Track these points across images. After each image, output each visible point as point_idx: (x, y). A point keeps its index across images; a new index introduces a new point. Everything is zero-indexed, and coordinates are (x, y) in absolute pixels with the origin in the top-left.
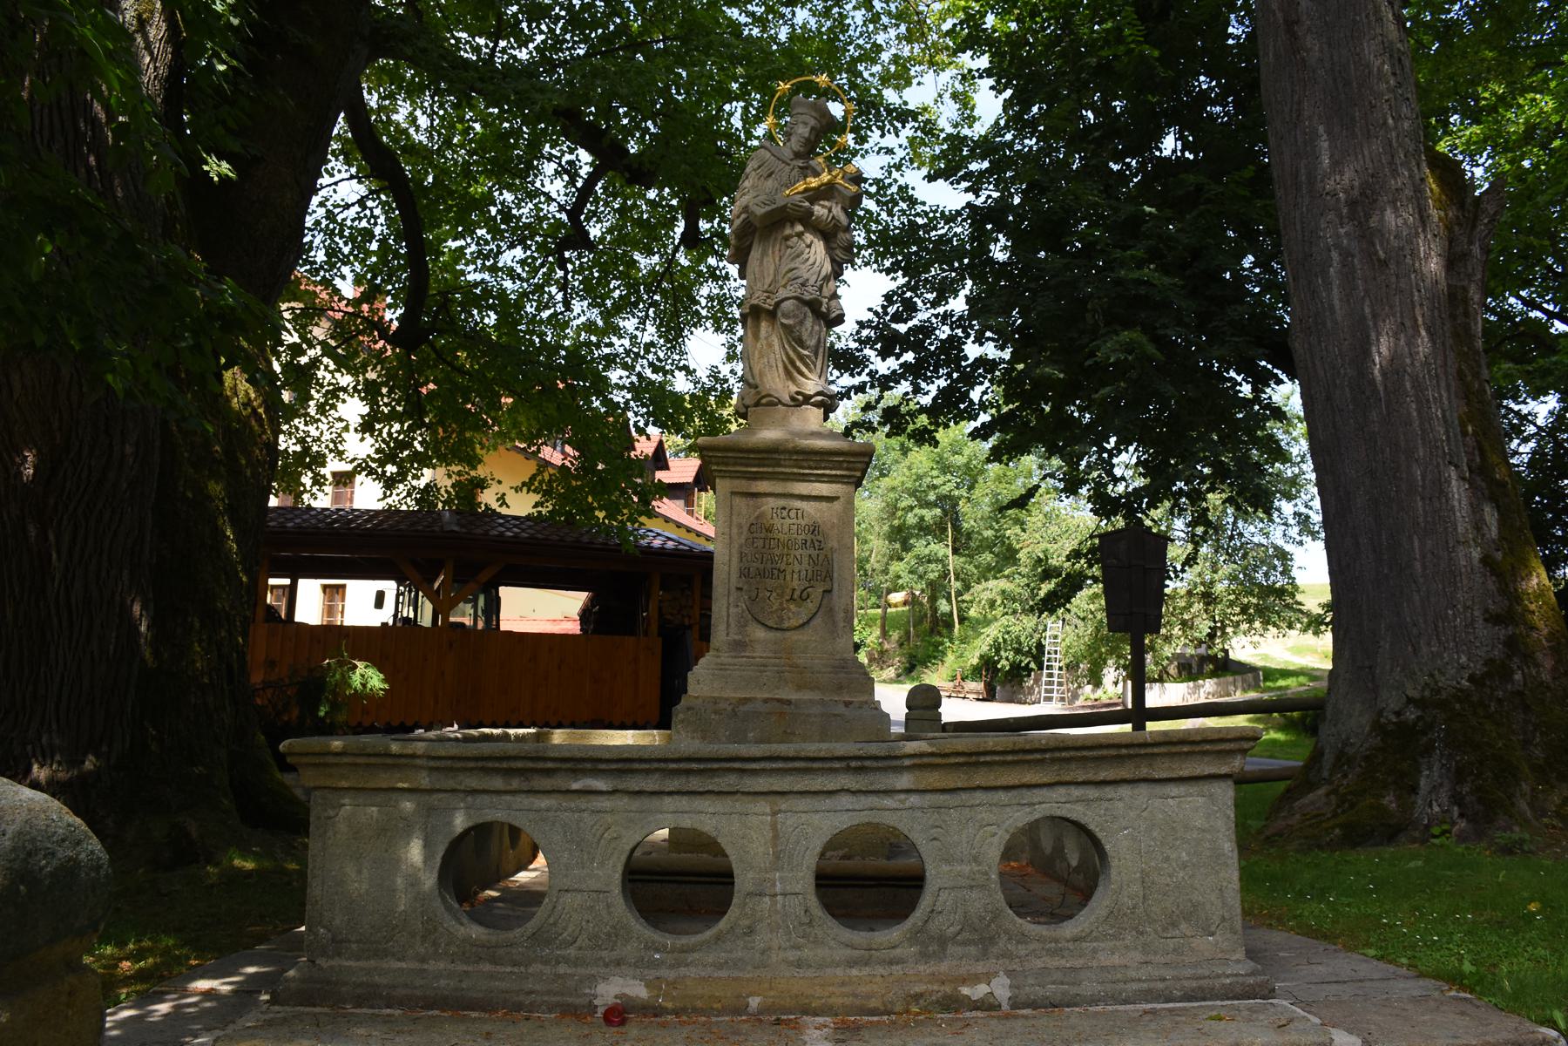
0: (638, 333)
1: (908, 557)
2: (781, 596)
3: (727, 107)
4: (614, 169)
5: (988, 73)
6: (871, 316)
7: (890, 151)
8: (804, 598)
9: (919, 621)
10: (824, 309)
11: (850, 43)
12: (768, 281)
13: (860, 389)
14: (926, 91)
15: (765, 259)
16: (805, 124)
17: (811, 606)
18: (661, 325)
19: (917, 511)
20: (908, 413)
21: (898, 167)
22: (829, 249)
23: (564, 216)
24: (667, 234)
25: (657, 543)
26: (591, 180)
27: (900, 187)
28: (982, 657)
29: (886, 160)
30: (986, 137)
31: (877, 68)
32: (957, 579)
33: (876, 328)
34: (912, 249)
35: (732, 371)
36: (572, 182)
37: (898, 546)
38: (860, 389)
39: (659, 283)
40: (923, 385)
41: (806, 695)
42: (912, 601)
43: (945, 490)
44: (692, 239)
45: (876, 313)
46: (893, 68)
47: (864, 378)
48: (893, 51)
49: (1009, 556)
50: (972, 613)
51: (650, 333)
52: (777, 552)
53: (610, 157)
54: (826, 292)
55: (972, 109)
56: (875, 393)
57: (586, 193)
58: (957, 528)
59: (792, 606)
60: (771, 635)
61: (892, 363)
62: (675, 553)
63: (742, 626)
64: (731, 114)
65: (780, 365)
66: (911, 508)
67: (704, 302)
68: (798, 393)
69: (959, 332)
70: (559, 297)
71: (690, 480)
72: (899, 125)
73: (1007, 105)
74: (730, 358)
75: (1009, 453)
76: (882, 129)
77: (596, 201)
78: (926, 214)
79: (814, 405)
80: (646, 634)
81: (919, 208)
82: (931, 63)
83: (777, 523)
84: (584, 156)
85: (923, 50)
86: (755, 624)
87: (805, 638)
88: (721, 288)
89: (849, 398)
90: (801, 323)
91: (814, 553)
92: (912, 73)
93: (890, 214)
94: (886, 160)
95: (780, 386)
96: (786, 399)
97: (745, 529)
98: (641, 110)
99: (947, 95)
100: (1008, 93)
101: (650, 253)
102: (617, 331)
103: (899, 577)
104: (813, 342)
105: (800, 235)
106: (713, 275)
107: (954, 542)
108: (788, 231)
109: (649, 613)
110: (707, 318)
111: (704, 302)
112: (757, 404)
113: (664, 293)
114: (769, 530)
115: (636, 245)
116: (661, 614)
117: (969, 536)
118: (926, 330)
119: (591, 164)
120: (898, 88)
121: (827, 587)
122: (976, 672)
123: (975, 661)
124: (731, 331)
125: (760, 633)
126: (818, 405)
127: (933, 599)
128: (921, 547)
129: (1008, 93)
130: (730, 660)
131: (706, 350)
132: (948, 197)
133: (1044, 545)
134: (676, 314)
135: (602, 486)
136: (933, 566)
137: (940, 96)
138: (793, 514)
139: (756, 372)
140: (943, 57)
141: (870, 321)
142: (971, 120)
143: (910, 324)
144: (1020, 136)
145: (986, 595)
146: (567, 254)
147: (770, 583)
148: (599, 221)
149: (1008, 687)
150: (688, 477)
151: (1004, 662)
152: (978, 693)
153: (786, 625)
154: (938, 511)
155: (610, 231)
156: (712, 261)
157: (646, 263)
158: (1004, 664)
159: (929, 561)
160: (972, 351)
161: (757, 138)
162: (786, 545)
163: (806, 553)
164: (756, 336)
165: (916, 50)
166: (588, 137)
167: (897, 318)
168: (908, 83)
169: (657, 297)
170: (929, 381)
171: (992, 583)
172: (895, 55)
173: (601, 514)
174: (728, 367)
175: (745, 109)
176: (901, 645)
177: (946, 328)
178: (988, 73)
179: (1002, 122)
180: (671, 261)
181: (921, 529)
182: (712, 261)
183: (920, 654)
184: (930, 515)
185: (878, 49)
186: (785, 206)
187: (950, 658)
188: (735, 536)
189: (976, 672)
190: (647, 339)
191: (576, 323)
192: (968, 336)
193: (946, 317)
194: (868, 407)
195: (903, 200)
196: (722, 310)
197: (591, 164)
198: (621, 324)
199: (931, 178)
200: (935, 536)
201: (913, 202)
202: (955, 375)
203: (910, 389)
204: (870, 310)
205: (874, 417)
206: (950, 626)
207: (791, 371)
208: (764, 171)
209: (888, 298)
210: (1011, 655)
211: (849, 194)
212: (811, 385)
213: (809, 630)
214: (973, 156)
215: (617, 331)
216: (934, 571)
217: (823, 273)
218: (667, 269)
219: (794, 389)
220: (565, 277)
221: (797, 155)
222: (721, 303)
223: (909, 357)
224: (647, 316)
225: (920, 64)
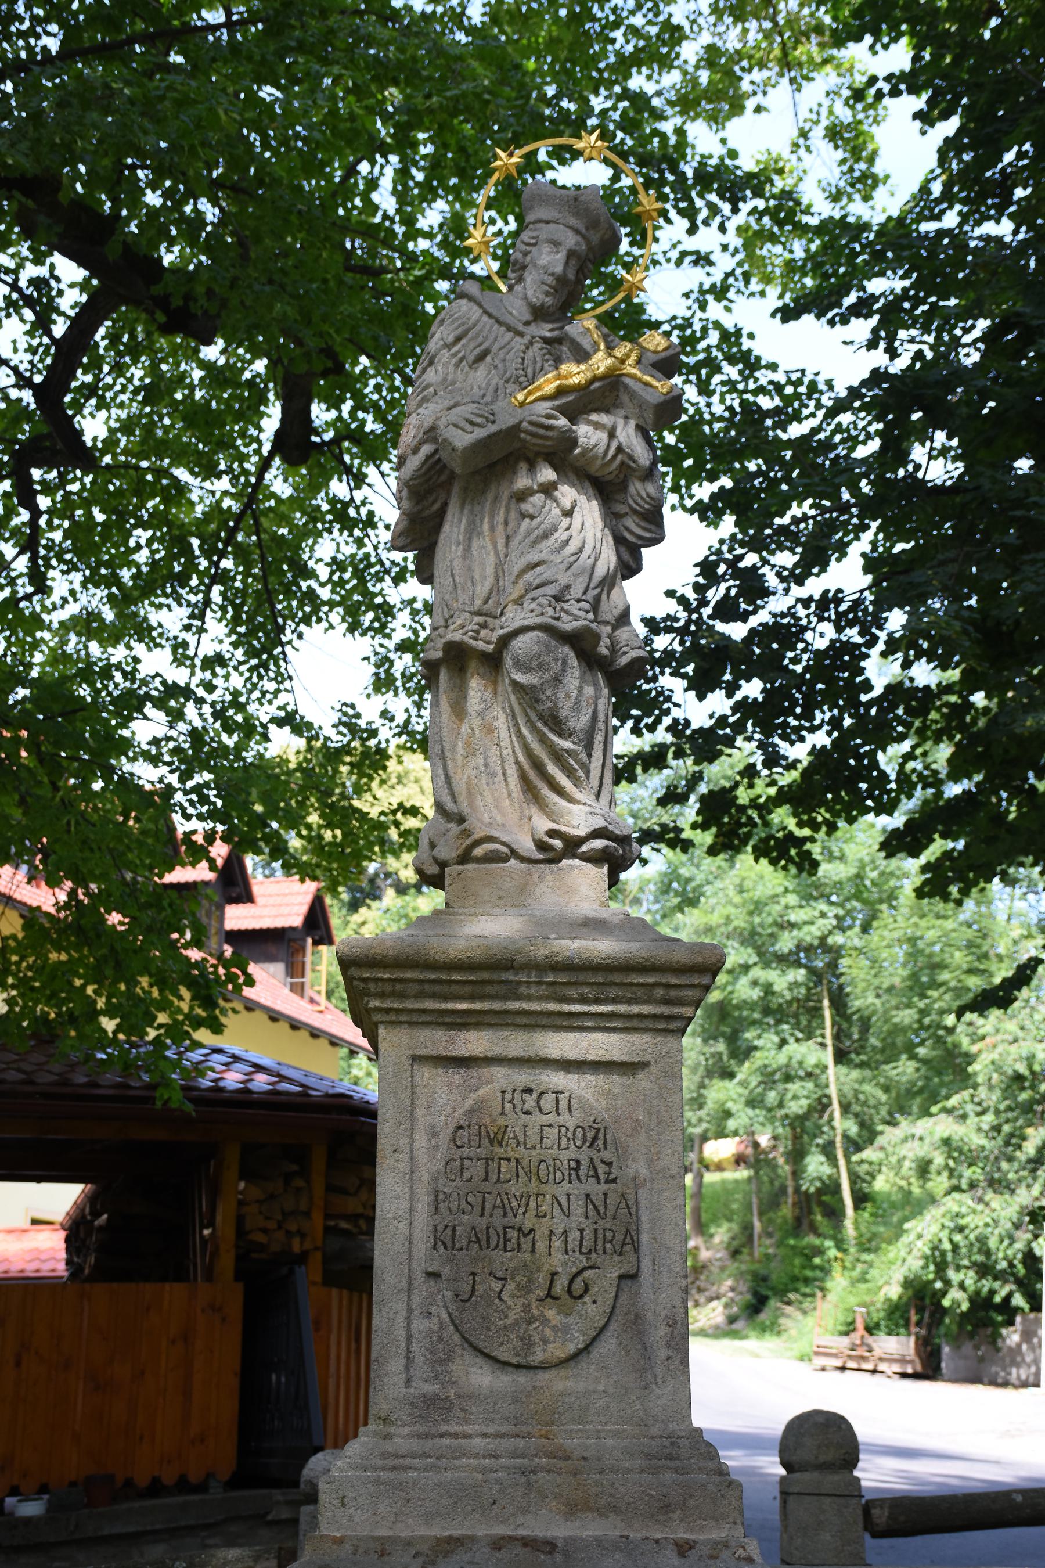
0: (191, 638)
1: (744, 1071)
2: (526, 1289)
3: (364, 167)
4: (134, 302)
5: (904, 83)
6: (672, 607)
7: (702, 259)
8: (576, 1292)
9: (772, 1202)
10: (603, 650)
11: (616, 25)
12: (483, 589)
13: (655, 759)
14: (770, 128)
15: (472, 547)
16: (556, 244)
17: (592, 1311)
18: (236, 621)
19: (757, 973)
20: (754, 803)
21: (720, 292)
22: (611, 517)
23: (27, 396)
24: (243, 434)
25: (233, 1079)
26: (84, 322)
27: (725, 336)
28: (907, 1283)
29: (694, 277)
30: (900, 220)
31: (672, 78)
32: (845, 1109)
33: (682, 632)
34: (765, 469)
35: (384, 714)
36: (43, 324)
37: (721, 1047)
38: (655, 759)
39: (232, 532)
40: (784, 747)
41: (589, 1528)
42: (752, 1158)
43: (810, 934)
44: (294, 443)
45: (683, 601)
46: (704, 77)
47: (662, 736)
48: (706, 39)
49: (951, 1068)
50: (881, 1184)
51: (216, 636)
52: (515, 1188)
53: (124, 279)
54: (610, 609)
55: (871, 160)
56: (687, 765)
57: (72, 350)
58: (839, 1001)
59: (550, 1313)
60: (506, 1380)
61: (719, 703)
62: (275, 1104)
63: (440, 1362)
64: (373, 184)
65: (512, 771)
66: (746, 968)
67: (323, 572)
68: (552, 833)
69: (853, 634)
70: (22, 564)
71: (297, 921)
72: (726, 208)
73: (948, 149)
74: (383, 683)
75: (961, 878)
76: (690, 213)
77: (96, 365)
78: (779, 388)
79: (588, 858)
80: (209, 1277)
81: (764, 377)
82: (786, 63)
83: (514, 1122)
84: (69, 271)
85: (767, 35)
86: (469, 1357)
87: (581, 1386)
88: (360, 543)
89: (632, 779)
90: (557, 681)
91: (597, 1189)
92: (745, 86)
93: (705, 390)
94: (694, 277)
95: (508, 818)
96: (526, 845)
97: (444, 1138)
98: (179, 171)
99: (818, 133)
100: (950, 126)
101: (210, 472)
102: (144, 632)
103: (728, 1114)
104: (580, 722)
105: (548, 490)
106: (342, 515)
107: (837, 1037)
108: (522, 482)
109: (217, 1230)
110: (332, 604)
111: (323, 572)
112: (465, 858)
113: (242, 555)
114: (496, 1140)
115: (182, 455)
116: (241, 1231)
117: (865, 1025)
118: (785, 633)
119: (84, 286)
120: (716, 119)
121: (627, 1268)
122: (896, 1317)
123: (894, 1291)
124: (381, 630)
125: (481, 1378)
126: (595, 858)
127: (797, 1156)
128: (769, 1049)
129: (950, 126)
130: (416, 1445)
131: (329, 673)
132: (835, 354)
133: (1025, 1048)
134: (267, 597)
135: (115, 960)
136: (794, 1087)
137: (804, 134)
138: (548, 1102)
139: (460, 783)
140: (810, 49)
141: (669, 618)
142: (867, 183)
143: (754, 621)
144: (974, 215)
145: (913, 1151)
146: (36, 474)
147: (502, 1260)
148: (102, 404)
149: (968, 1347)
150: (294, 917)
151: (955, 1294)
152: (902, 1360)
153: (538, 1356)
154: (800, 975)
155: (127, 427)
156: (339, 488)
157: (207, 492)
158: (956, 1299)
159: (788, 1078)
160: (880, 672)
161: (429, 235)
162: (533, 1173)
163: (577, 1189)
164: (459, 710)
165: (753, 36)
166: (81, 233)
167: (727, 610)
168: (737, 108)
169: (227, 563)
170: (794, 736)
171: (923, 1126)
172: (711, 48)
173: (109, 1025)
174: (378, 702)
175: (403, 174)
176: (735, 1253)
177: (828, 630)
178: (904, 83)
179: (937, 189)
180: (252, 494)
181: (767, 1011)
182: (339, 488)
183: (777, 1274)
184: (785, 981)
185: (674, 34)
186: (516, 428)
187: (838, 1282)
188: (422, 1156)
189: (896, 1317)
190: (208, 648)
191: (56, 618)
192: (873, 641)
193: (826, 602)
194: (672, 797)
195: (731, 360)
196: (361, 586)
197: (84, 286)
198: (154, 617)
199: (787, 314)
200: (797, 1026)
201: (750, 363)
202: (847, 722)
203: (758, 758)
204: (670, 594)
205: (689, 813)
206: (835, 1214)
207: (535, 783)
208: (468, 348)
209: (707, 568)
210: (970, 1278)
211: (653, 398)
212: (579, 817)
213: (588, 1367)
214: (878, 265)
215: (144, 632)
216: (798, 1098)
217: (600, 571)
218: (247, 506)
219: (542, 824)
220: (33, 523)
221: (539, 313)
222: (358, 574)
223: (753, 689)
224: (207, 602)
225: (762, 65)
